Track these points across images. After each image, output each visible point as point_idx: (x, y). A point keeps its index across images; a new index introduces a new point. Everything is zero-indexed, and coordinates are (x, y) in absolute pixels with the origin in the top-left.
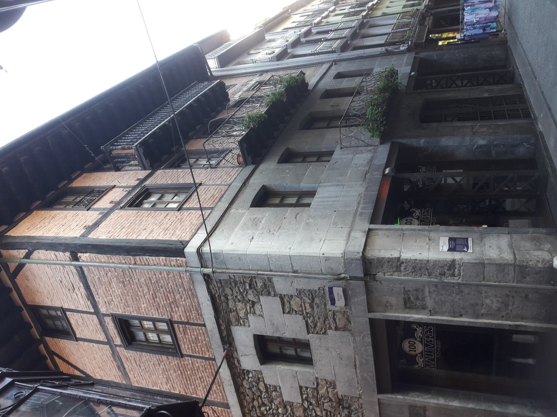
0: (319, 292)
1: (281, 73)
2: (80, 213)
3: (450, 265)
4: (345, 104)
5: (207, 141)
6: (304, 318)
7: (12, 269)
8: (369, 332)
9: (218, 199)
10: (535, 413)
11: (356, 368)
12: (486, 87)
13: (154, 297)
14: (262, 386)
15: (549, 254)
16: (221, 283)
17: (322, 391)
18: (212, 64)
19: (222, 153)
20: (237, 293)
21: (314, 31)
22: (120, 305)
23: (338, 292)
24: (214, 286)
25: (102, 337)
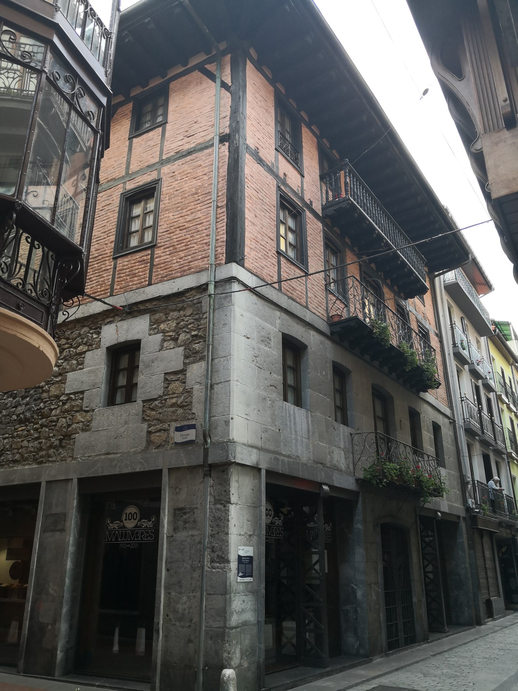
0: (189, 414)
1: (438, 358)
2: (272, 141)
3: (223, 558)
4: (404, 437)
5: (357, 280)
6: (160, 396)
7: (208, 67)
8: (147, 469)
9: (291, 295)
10: (61, 652)
11: (106, 454)
12: (424, 600)
13: (181, 228)
14: (81, 348)
15: (237, 665)
16: (198, 303)
17: (79, 417)
18: (450, 276)
19: (343, 294)
20: (187, 321)
21: (492, 395)
22: (171, 189)
23: (191, 435)
24: (195, 296)
25: (134, 167)
